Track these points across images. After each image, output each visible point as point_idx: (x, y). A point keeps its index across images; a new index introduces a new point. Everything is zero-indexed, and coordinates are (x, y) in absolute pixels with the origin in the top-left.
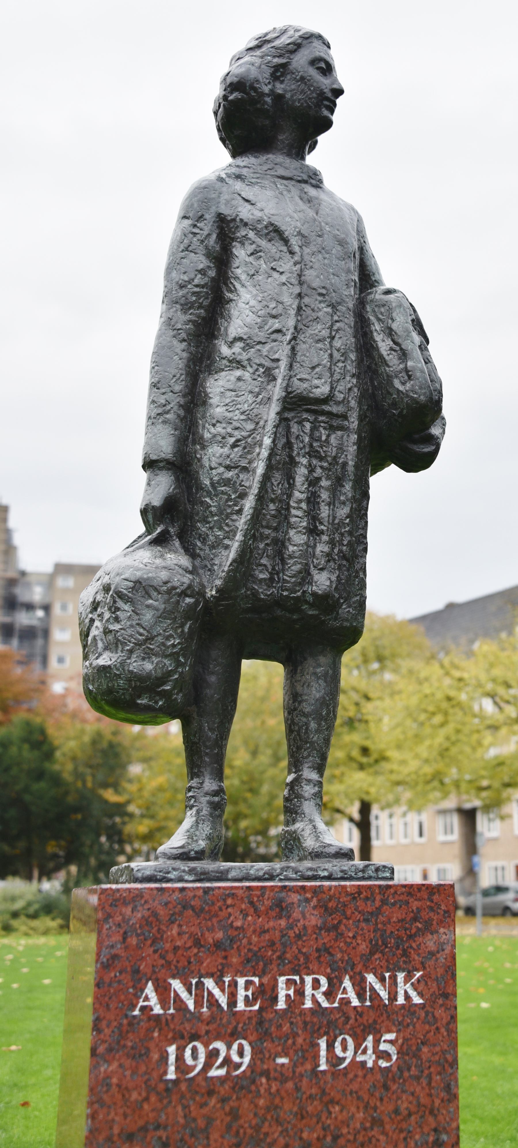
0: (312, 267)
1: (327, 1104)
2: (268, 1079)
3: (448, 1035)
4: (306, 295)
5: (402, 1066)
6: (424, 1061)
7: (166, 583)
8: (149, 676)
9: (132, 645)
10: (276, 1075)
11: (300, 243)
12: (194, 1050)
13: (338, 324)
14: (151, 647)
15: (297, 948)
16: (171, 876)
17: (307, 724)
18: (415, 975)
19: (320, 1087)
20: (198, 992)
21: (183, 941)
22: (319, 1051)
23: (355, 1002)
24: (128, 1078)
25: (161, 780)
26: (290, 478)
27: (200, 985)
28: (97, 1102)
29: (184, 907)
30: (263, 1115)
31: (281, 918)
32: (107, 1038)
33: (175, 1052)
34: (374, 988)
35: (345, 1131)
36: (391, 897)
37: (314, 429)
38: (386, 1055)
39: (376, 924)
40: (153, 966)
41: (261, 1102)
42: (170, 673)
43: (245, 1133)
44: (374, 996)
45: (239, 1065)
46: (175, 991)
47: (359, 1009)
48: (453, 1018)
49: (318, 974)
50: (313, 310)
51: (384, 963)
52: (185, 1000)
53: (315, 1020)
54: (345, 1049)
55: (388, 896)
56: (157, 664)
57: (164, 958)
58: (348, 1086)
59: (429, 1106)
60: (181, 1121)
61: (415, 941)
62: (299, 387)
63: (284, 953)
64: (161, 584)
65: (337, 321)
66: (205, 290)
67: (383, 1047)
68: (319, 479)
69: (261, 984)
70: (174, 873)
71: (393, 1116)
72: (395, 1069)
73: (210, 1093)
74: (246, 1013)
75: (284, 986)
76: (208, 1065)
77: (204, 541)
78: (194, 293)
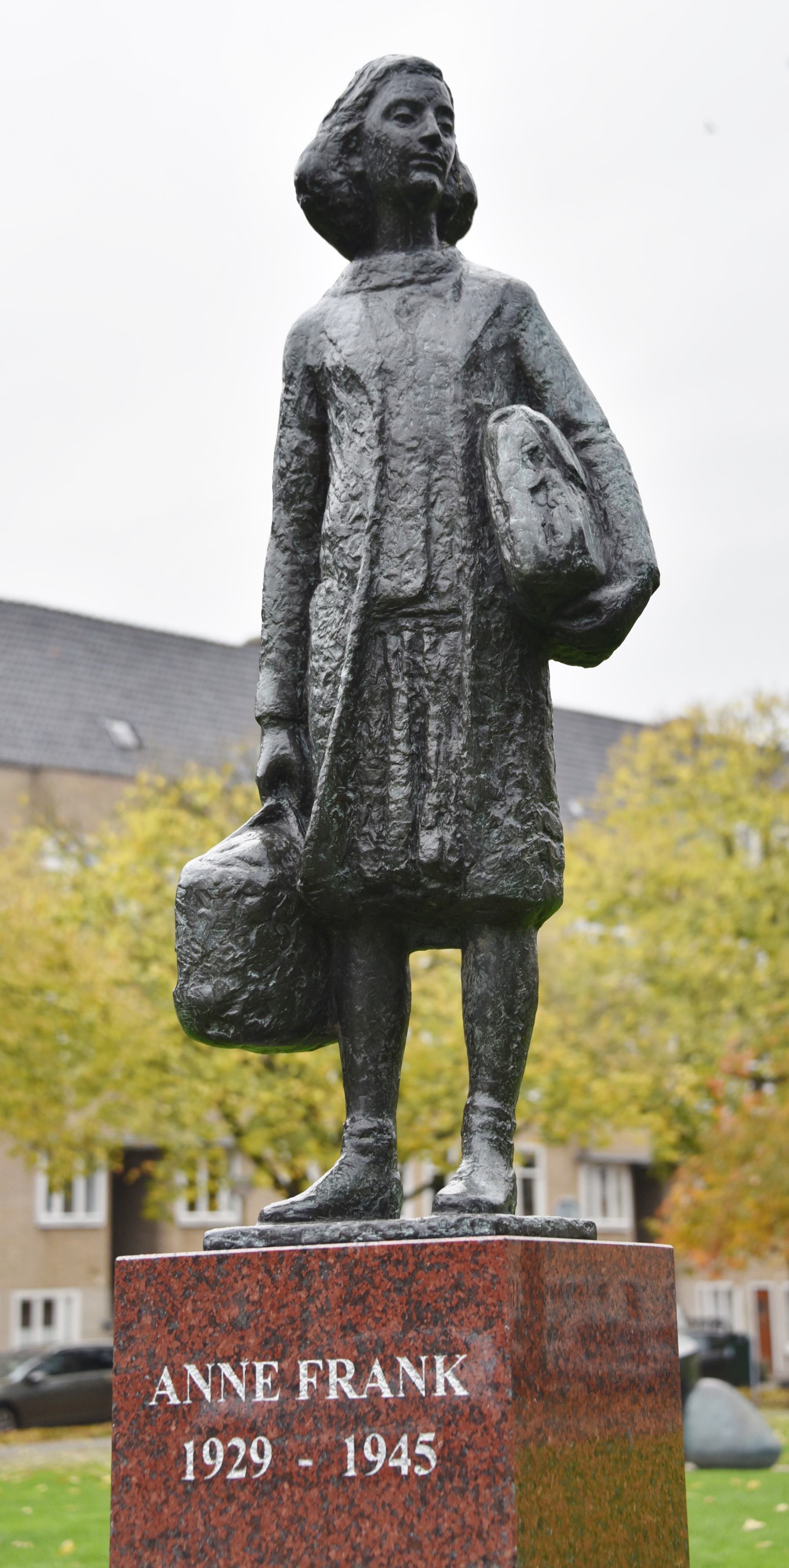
0: (398, 414)
1: (356, 1518)
3: (498, 1436)
4: (393, 456)
5: (443, 1474)
6: (469, 1469)
8: (207, 1002)
9: (188, 966)
10: (299, 1480)
11: (380, 386)
12: (213, 1447)
13: (439, 483)
14: (209, 965)
15: (319, 1326)
16: (238, 1242)
18: (457, 1359)
19: (348, 1497)
20: (214, 1379)
21: (197, 1319)
22: (346, 1452)
23: (387, 1393)
24: (147, 1477)
27: (216, 1371)
28: (118, 1503)
30: (286, 1527)
31: (300, 1290)
32: (126, 1431)
33: (192, 1449)
34: (408, 1376)
35: (377, 1552)
36: (427, 1259)
38: (422, 1460)
39: (410, 1295)
40: (168, 1349)
42: (233, 995)
43: (267, 1547)
44: (408, 1385)
46: (191, 1378)
47: (391, 1402)
49: (344, 1357)
50: (400, 475)
52: (201, 1388)
53: (341, 1414)
54: (375, 1451)
55: (423, 1259)
56: (215, 985)
57: (179, 1340)
58: (380, 1497)
59: (476, 1528)
60: (201, 1529)
61: (456, 1315)
62: (386, 585)
63: (306, 1331)
64: (212, 886)
65: (437, 480)
66: (304, 475)
67: (420, 1450)
69: (281, 1370)
70: (244, 1238)
71: (433, 1537)
72: (434, 1478)
73: (230, 1498)
74: (266, 1405)
75: (306, 1372)
76: (226, 1467)
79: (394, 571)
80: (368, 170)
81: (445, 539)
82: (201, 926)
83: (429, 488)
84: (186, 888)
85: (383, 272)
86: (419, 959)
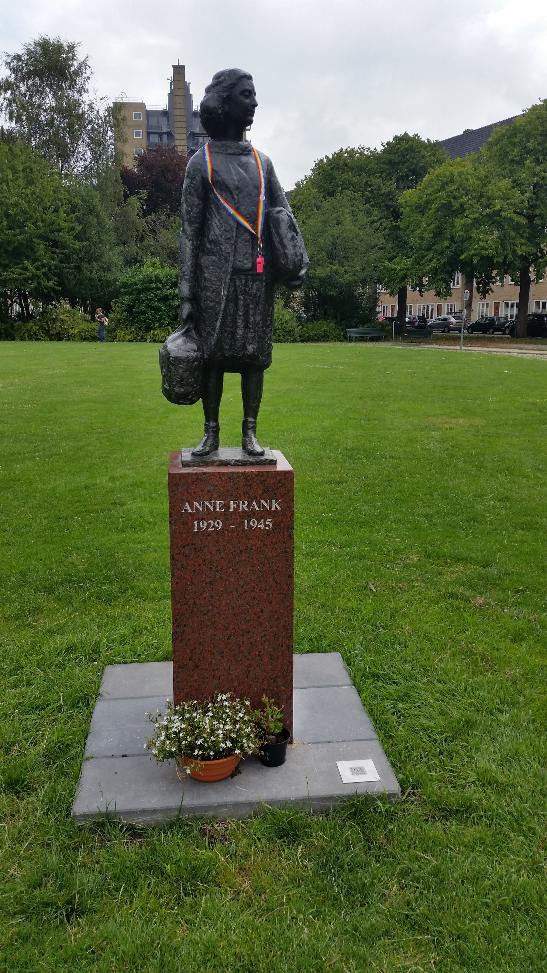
26: (236, 305)
38: (268, 526)
68: (248, 305)
73: (209, 535)
76: (207, 527)
79: (241, 259)
86: (227, 376)
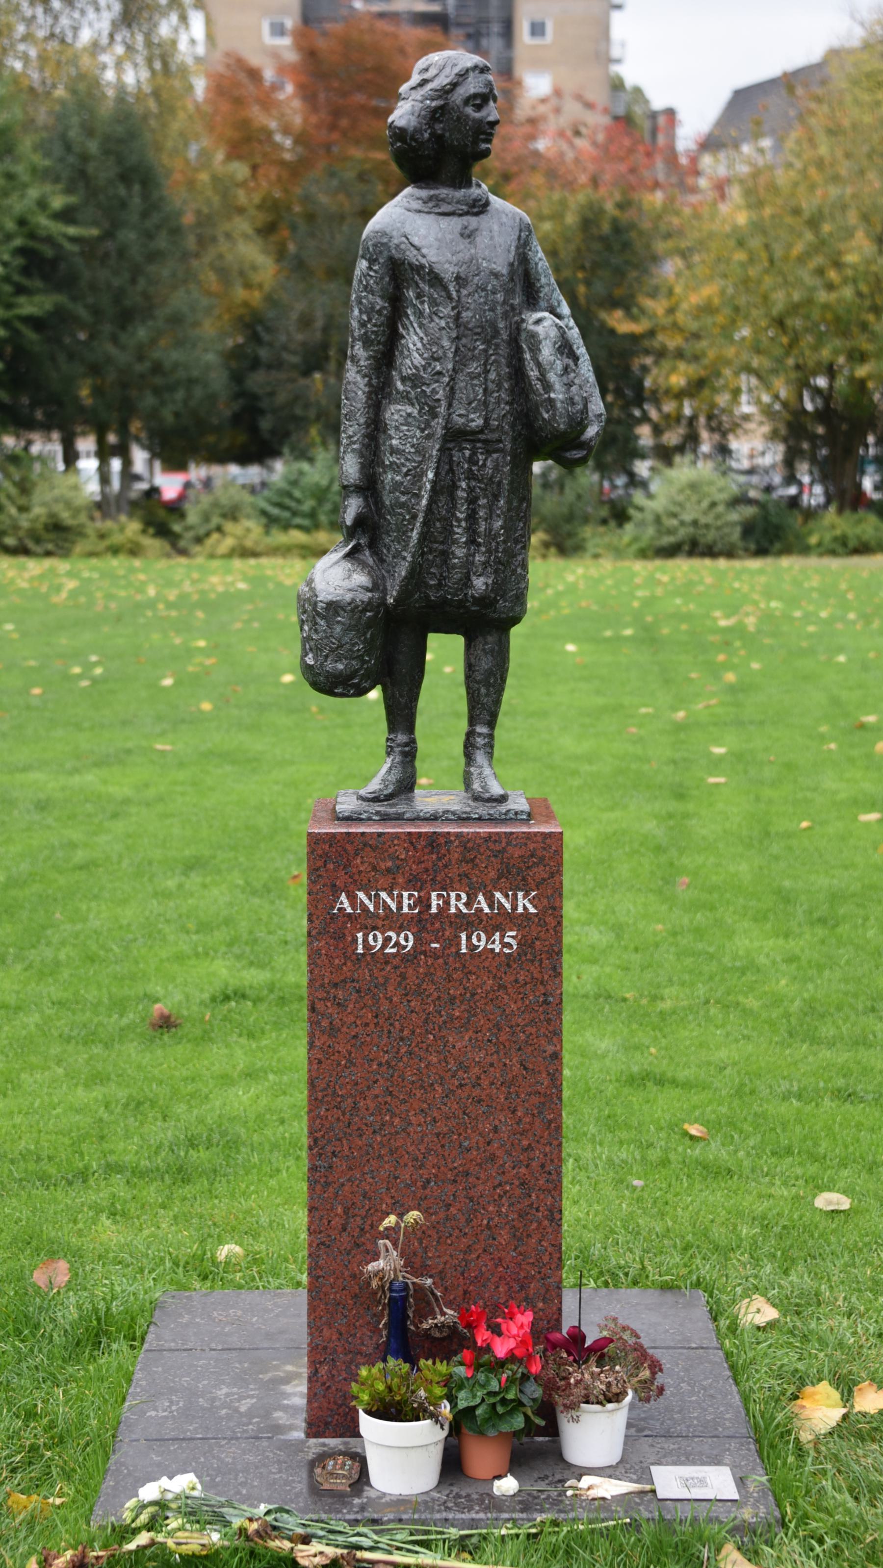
2: (426, 956)
5: (521, 952)
7: (350, 604)
12: (375, 936)
16: (363, 816)
17: (479, 690)
23: (487, 910)
25: (709, 291)
26: (453, 498)
27: (377, 896)
29: (365, 845)
35: (479, 991)
37: (474, 453)
38: (509, 946)
41: (421, 970)
42: (357, 671)
45: (406, 947)
48: (560, 923)
51: (508, 885)
54: (479, 940)
67: (506, 940)
69: (420, 897)
73: (387, 963)
76: (384, 946)
77: (388, 550)
78: (373, 332)
80: (447, 134)
81: (496, 395)
82: (338, 629)
83: (486, 361)
84: (327, 604)
85: (449, 203)
